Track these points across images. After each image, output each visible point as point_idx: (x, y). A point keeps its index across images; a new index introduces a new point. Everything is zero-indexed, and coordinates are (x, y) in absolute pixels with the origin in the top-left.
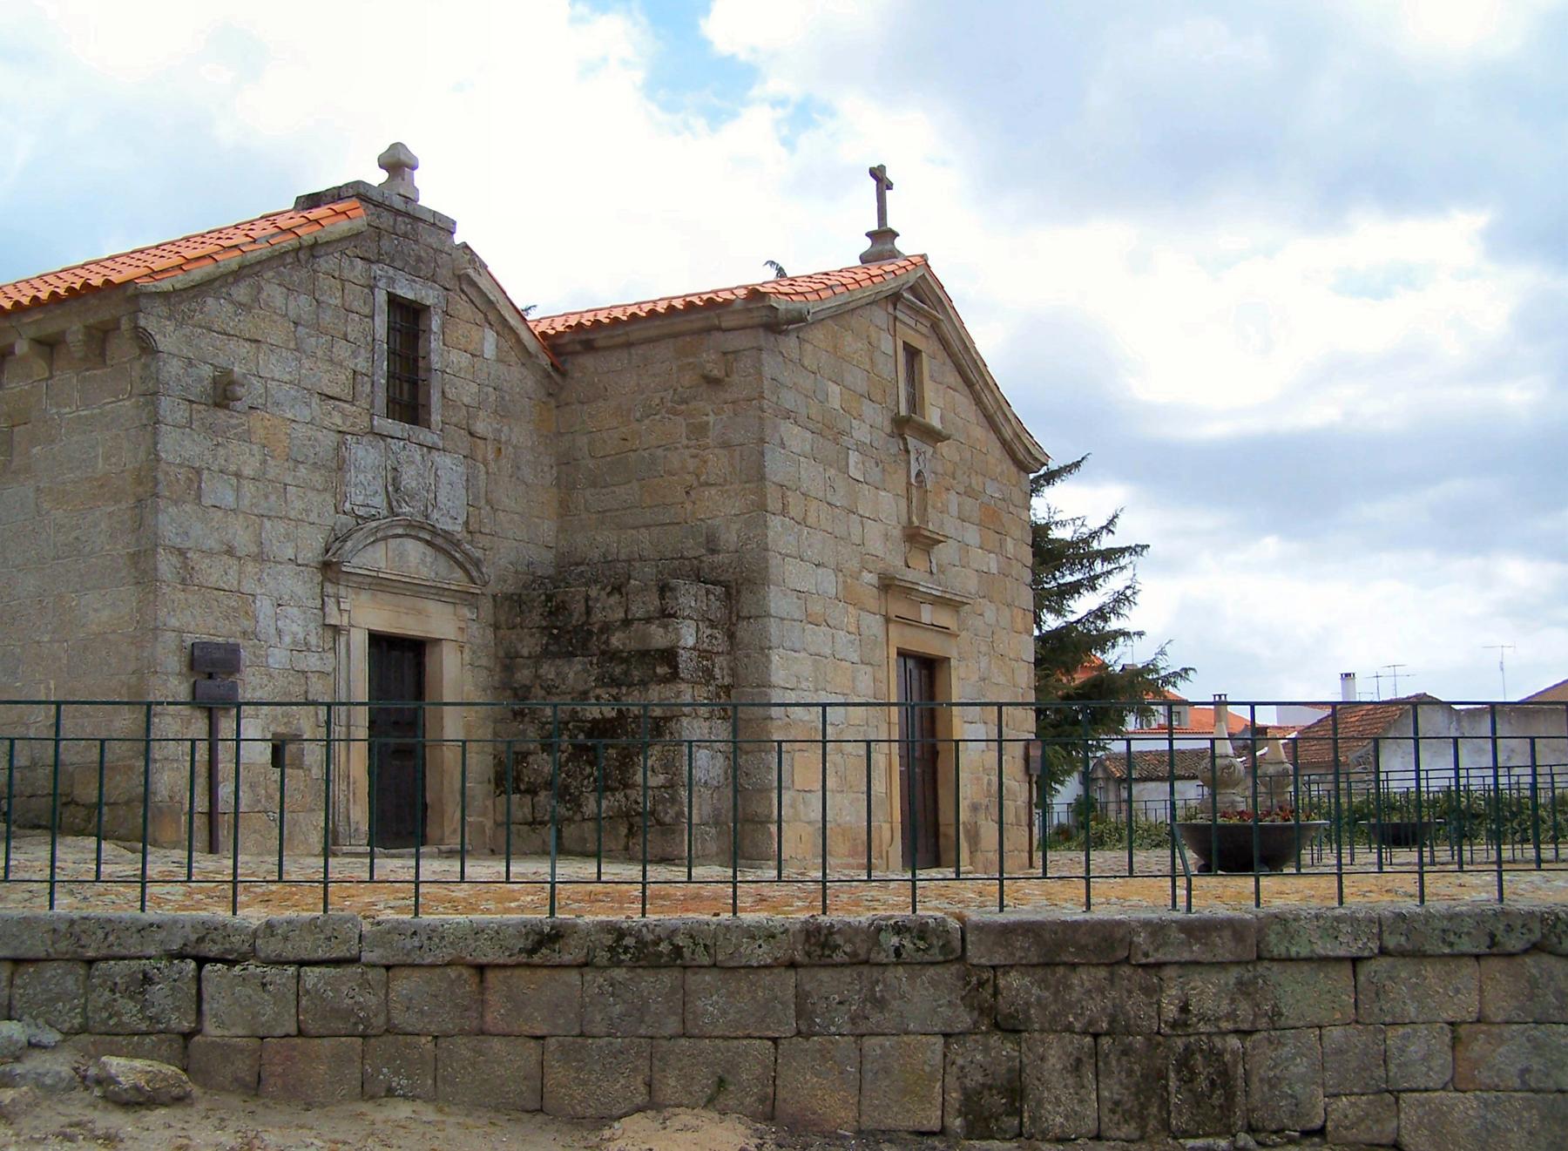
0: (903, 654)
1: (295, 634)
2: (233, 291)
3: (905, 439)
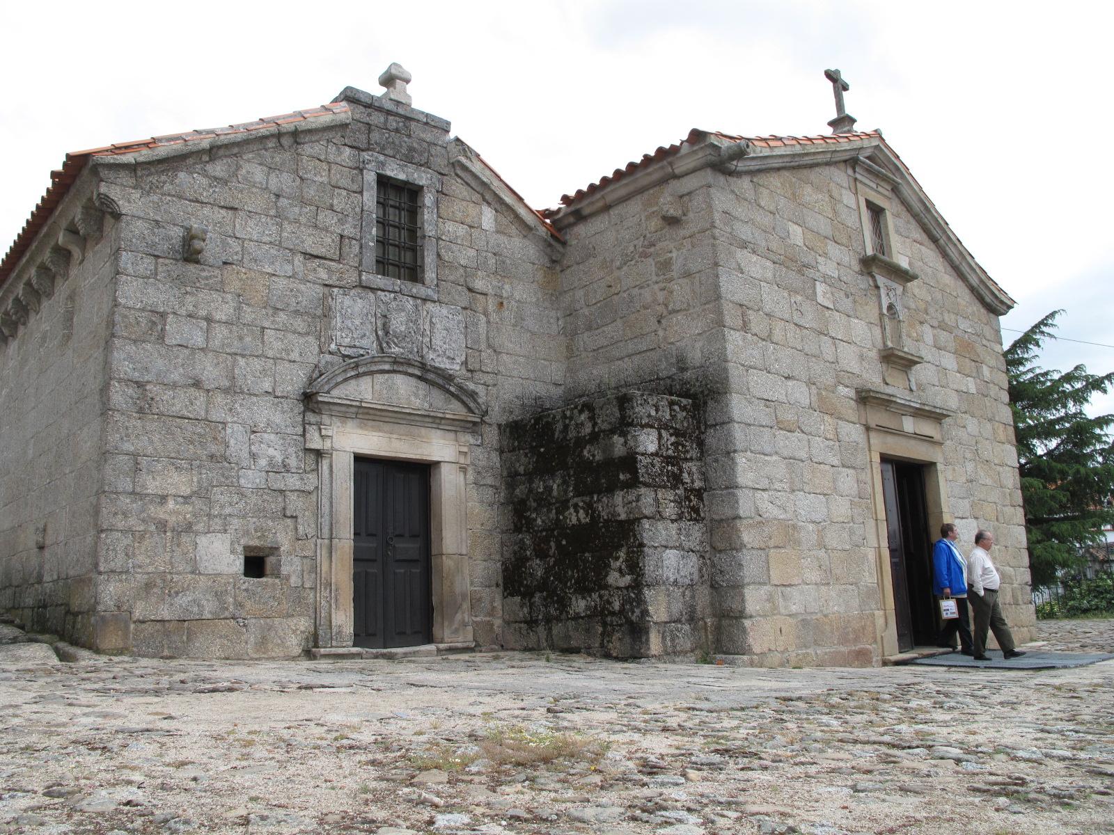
0: (885, 459)
1: (271, 458)
2: (209, 167)
3: (873, 277)
